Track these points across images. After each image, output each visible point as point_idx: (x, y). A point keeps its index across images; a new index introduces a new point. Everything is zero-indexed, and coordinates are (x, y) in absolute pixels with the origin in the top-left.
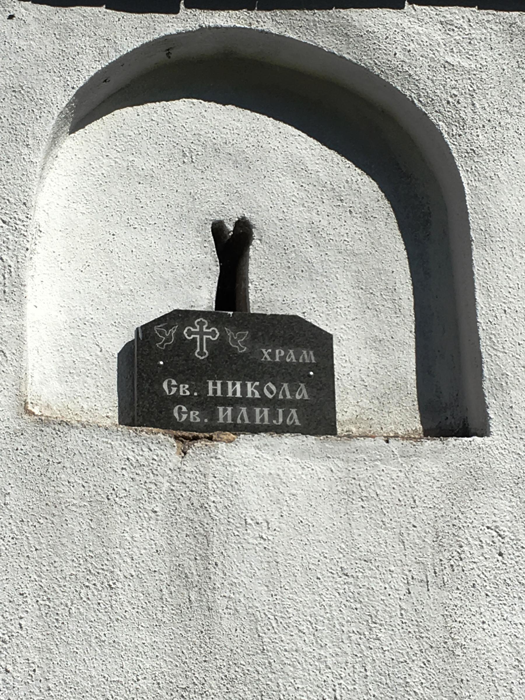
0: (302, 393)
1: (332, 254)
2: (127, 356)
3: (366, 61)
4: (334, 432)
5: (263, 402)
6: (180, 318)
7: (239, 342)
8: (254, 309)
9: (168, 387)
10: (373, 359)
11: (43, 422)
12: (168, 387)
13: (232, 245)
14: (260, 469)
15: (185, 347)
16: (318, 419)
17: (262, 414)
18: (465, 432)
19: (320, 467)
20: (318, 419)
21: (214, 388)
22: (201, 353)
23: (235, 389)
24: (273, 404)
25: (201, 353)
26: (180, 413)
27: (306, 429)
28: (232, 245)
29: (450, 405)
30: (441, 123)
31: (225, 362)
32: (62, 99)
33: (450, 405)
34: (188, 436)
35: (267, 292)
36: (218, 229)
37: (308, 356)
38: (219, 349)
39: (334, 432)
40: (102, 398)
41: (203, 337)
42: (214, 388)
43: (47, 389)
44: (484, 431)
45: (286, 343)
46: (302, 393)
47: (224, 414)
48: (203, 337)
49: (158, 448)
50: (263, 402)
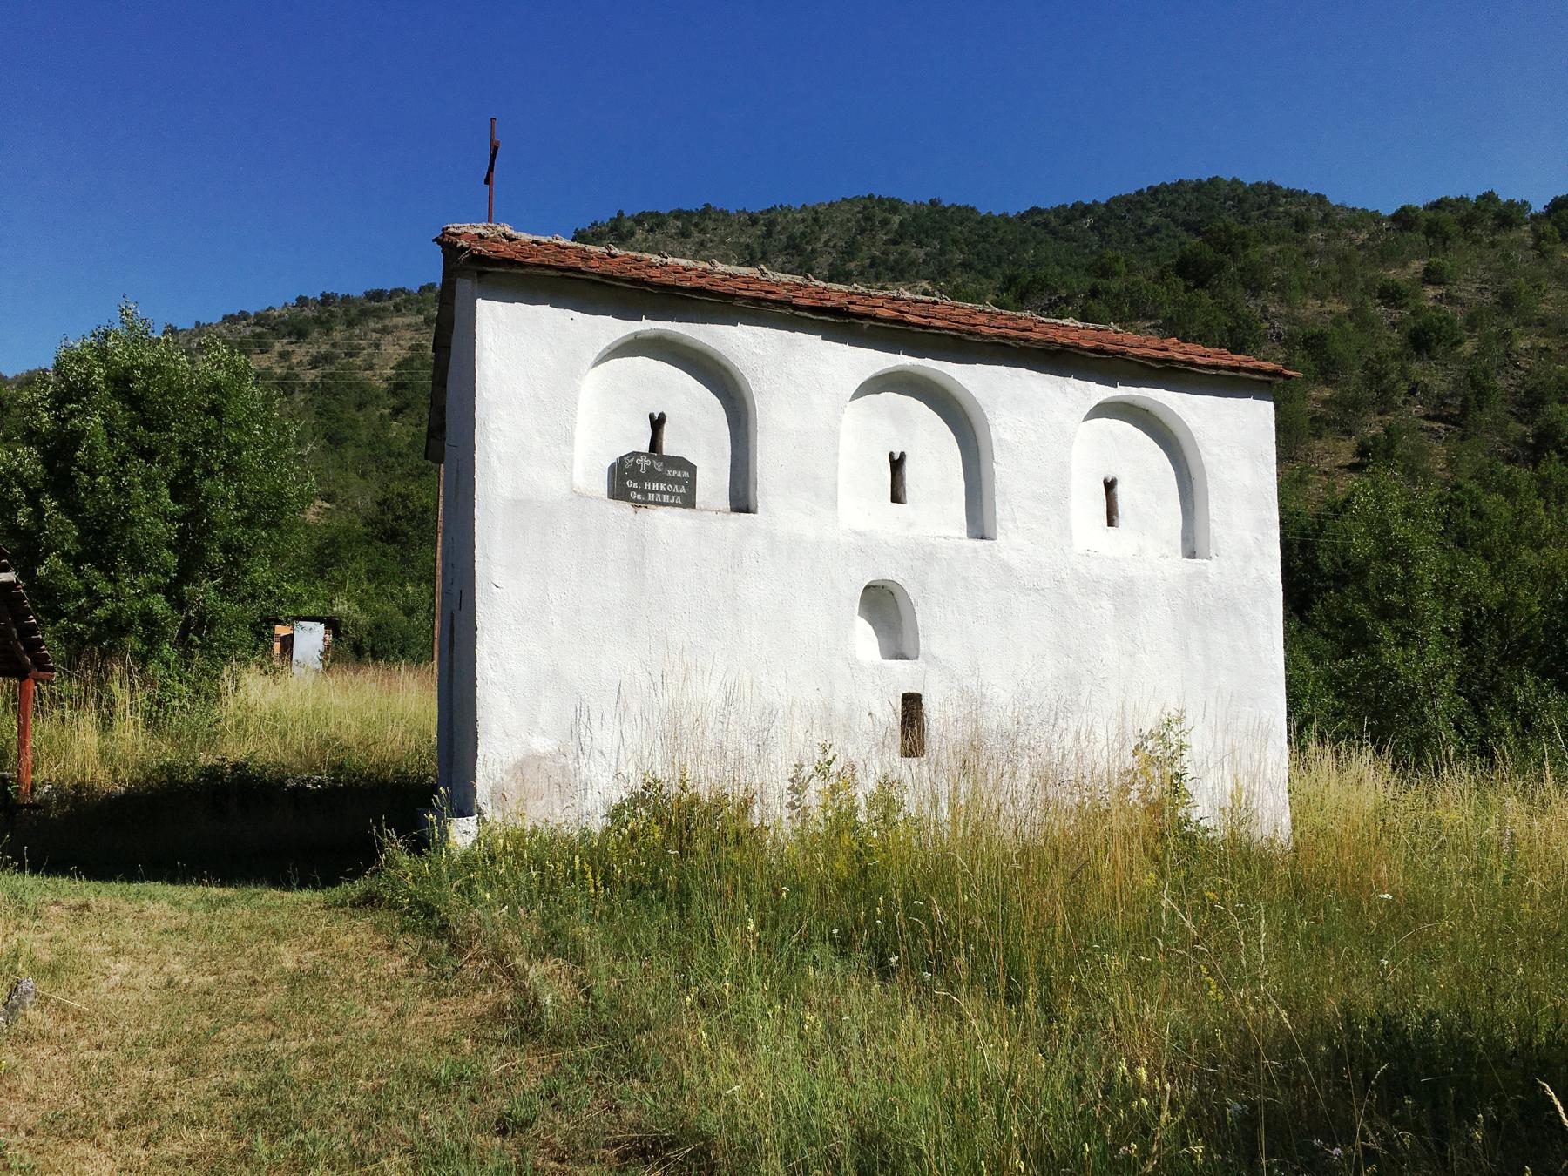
0: (683, 490)
1: (699, 430)
2: (612, 468)
3: (719, 349)
4: (694, 506)
5: (667, 492)
6: (636, 455)
7: (659, 466)
8: (1237, 436)
9: (629, 483)
10: (713, 480)
11: (581, 495)
12: (629, 483)
13: (657, 423)
14: (665, 520)
15: (636, 467)
16: (689, 502)
17: (666, 498)
18: (747, 511)
19: (689, 522)
20: (689, 502)
21: (647, 485)
22: (643, 470)
23: (656, 486)
24: (671, 494)
25: (643, 470)
26: (633, 495)
27: (683, 506)
28: (657, 423)
29: (741, 502)
30: (1080, 325)
31: (652, 475)
32: (592, 358)
33: (741, 502)
34: (638, 504)
35: (670, 447)
36: (651, 416)
37: (686, 475)
38: (651, 469)
39: (694, 506)
40: (601, 486)
41: (644, 463)
42: (647, 485)
43: (580, 481)
44: (754, 512)
45: (679, 468)
46: (683, 490)
47: (651, 497)
48: (644, 463)
49: (624, 508)
50: (667, 492)
